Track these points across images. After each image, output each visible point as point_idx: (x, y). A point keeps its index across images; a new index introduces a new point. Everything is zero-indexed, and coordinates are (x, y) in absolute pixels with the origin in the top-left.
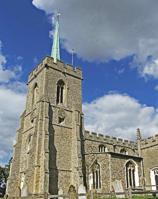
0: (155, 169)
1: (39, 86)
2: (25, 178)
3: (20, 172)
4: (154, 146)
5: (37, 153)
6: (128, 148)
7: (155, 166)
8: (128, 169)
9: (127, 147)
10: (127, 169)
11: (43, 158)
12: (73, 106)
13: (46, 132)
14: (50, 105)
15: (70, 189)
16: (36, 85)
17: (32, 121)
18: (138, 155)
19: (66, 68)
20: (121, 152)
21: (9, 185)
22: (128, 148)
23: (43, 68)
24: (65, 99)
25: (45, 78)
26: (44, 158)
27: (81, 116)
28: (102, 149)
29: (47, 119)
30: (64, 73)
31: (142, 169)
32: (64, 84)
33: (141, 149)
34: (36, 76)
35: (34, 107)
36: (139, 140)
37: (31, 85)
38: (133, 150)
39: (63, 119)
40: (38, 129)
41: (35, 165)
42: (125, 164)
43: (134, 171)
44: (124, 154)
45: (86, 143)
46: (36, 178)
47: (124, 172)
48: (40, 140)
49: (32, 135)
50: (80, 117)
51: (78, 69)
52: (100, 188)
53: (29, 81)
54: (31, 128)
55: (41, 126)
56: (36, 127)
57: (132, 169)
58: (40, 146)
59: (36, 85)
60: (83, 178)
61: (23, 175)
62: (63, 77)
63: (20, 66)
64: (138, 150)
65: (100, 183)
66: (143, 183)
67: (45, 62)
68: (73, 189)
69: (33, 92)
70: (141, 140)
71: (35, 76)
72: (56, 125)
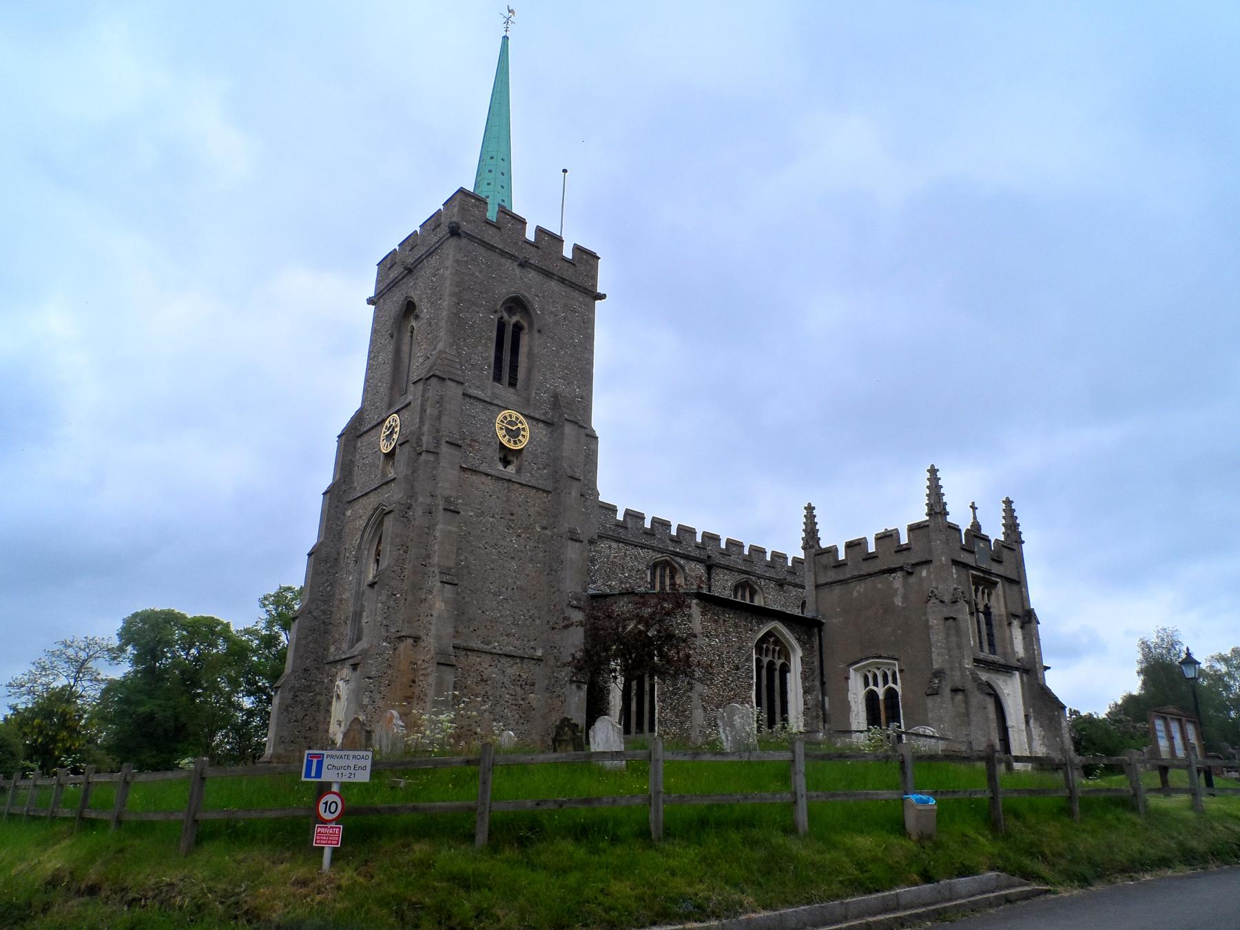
2: (353, 684)
6: (766, 578)
8: (765, 660)
10: (758, 661)
15: (558, 734)
18: (804, 604)
22: (766, 578)
25: (448, 283)
28: (662, 576)
33: (817, 586)
43: (785, 669)
47: (749, 670)
52: (652, 730)
57: (779, 663)
61: (346, 672)
63: (795, 560)
64: (803, 587)
68: (570, 733)
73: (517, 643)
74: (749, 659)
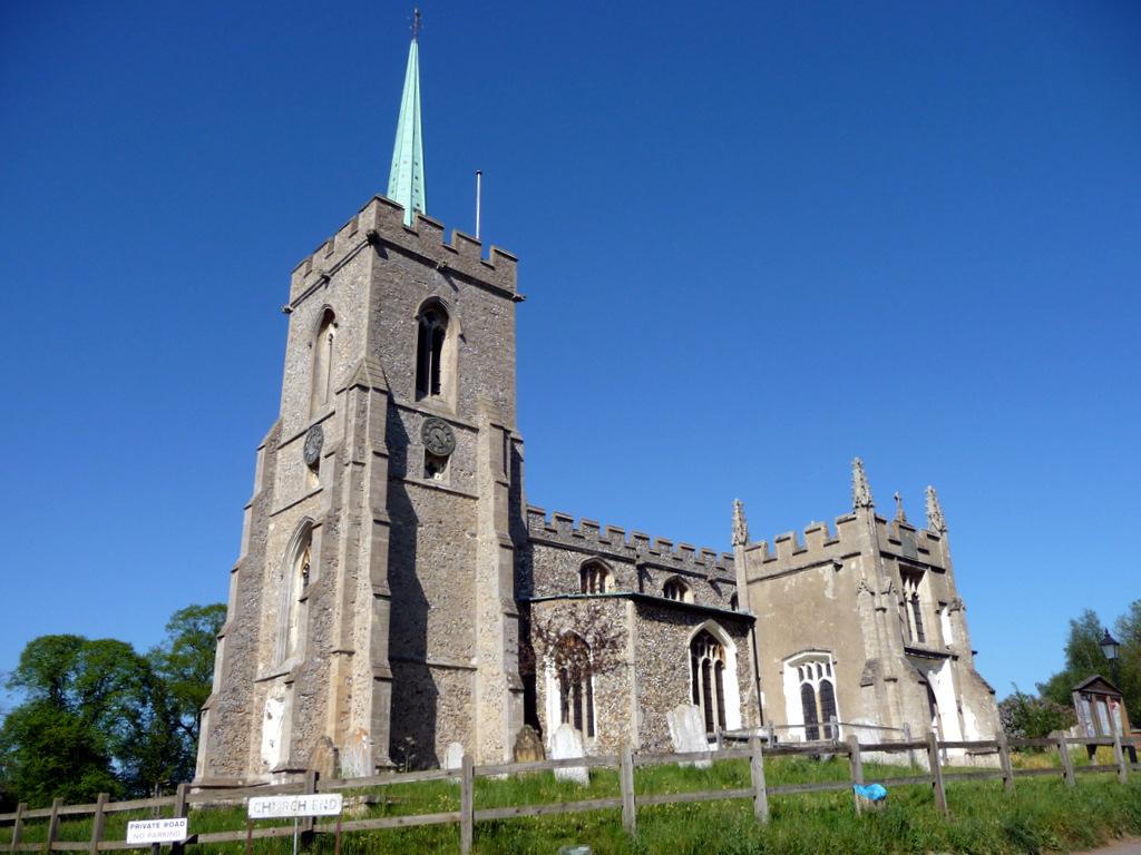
0: (802, 662)
1: (340, 324)
3: (260, 677)
4: (801, 569)
5: (338, 600)
7: (807, 646)
9: (689, 574)
11: (364, 621)
12: (482, 408)
13: (375, 511)
14: (391, 403)
16: (328, 317)
17: (314, 467)
19: (456, 252)
20: (665, 589)
21: (215, 730)
23: (358, 249)
24: (450, 376)
26: (366, 621)
27: (513, 448)
28: (593, 579)
29: (379, 459)
30: (446, 272)
31: (751, 659)
32: (445, 317)
33: (749, 583)
34: (327, 280)
35: (318, 408)
36: (741, 546)
37: (303, 316)
38: (711, 582)
39: (444, 460)
40: (345, 499)
41: (333, 649)
42: (688, 643)
43: (719, 666)
44: (678, 599)
45: (541, 554)
46: (338, 700)
47: (685, 669)
48: (353, 544)
49: (320, 525)
50: (509, 451)
51: (463, 237)
53: (294, 295)
54: (311, 496)
55: (357, 487)
56: (336, 492)
57: (714, 660)
58: (352, 571)
59: (328, 317)
60: (522, 696)
62: (439, 287)
65: (590, 716)
66: (754, 712)
67: (368, 220)
69: (314, 344)
70: (748, 547)
71: (323, 277)
72: (414, 484)
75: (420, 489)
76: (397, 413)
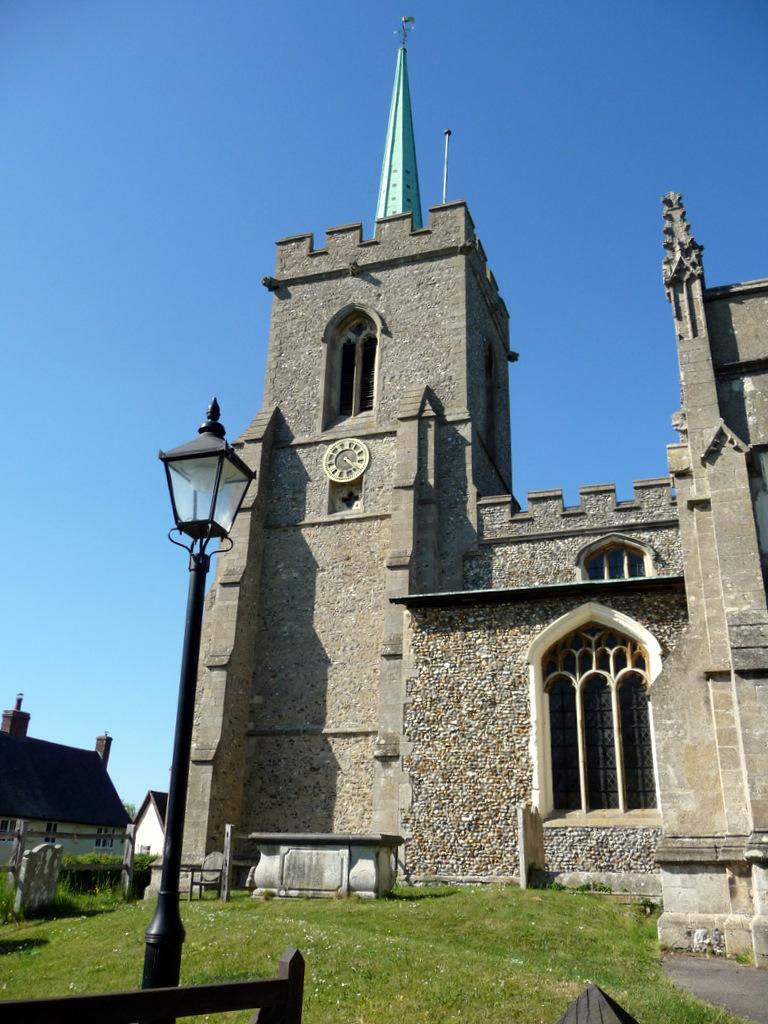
73: (360, 716)
74: (519, 683)
75: (321, 528)
76: (295, 453)
